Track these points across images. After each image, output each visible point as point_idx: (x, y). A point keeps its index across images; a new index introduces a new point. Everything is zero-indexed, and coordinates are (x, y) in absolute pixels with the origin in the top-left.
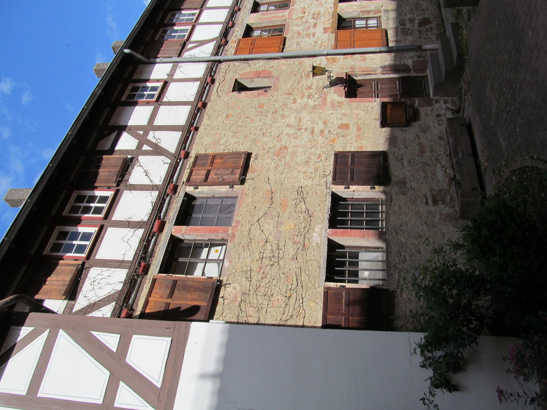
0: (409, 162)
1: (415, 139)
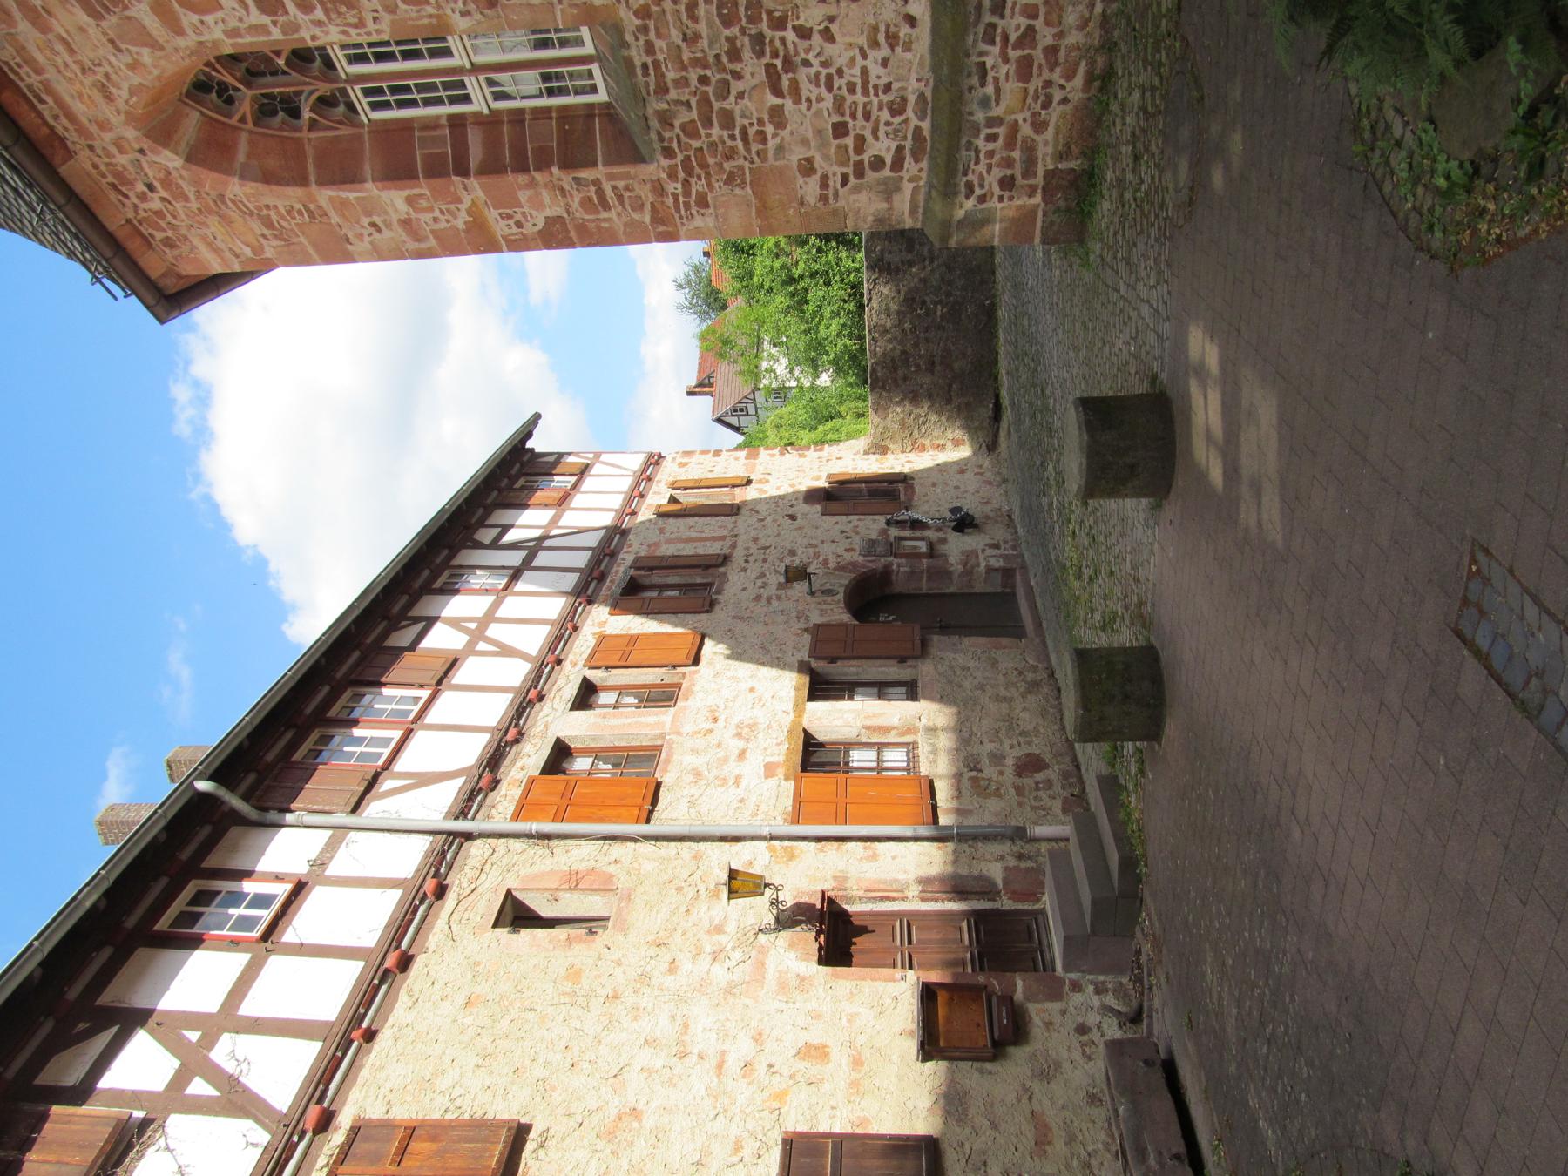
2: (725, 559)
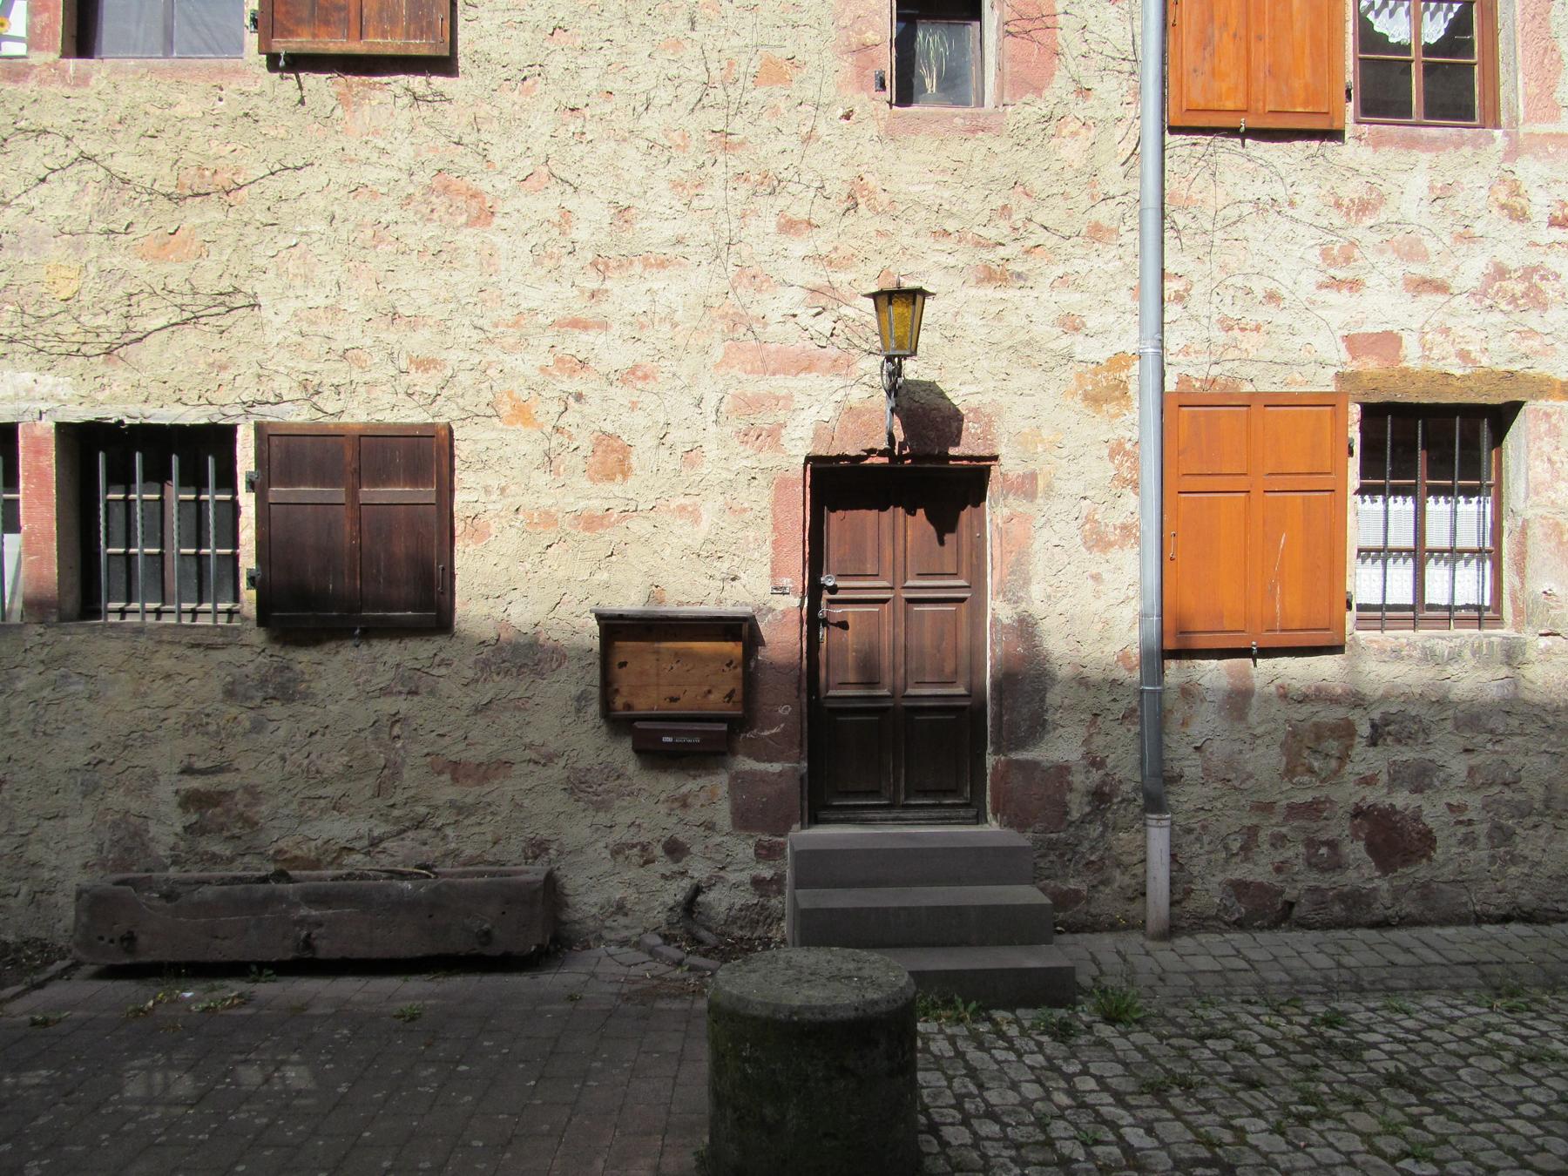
0: (396, 719)
1: (530, 746)
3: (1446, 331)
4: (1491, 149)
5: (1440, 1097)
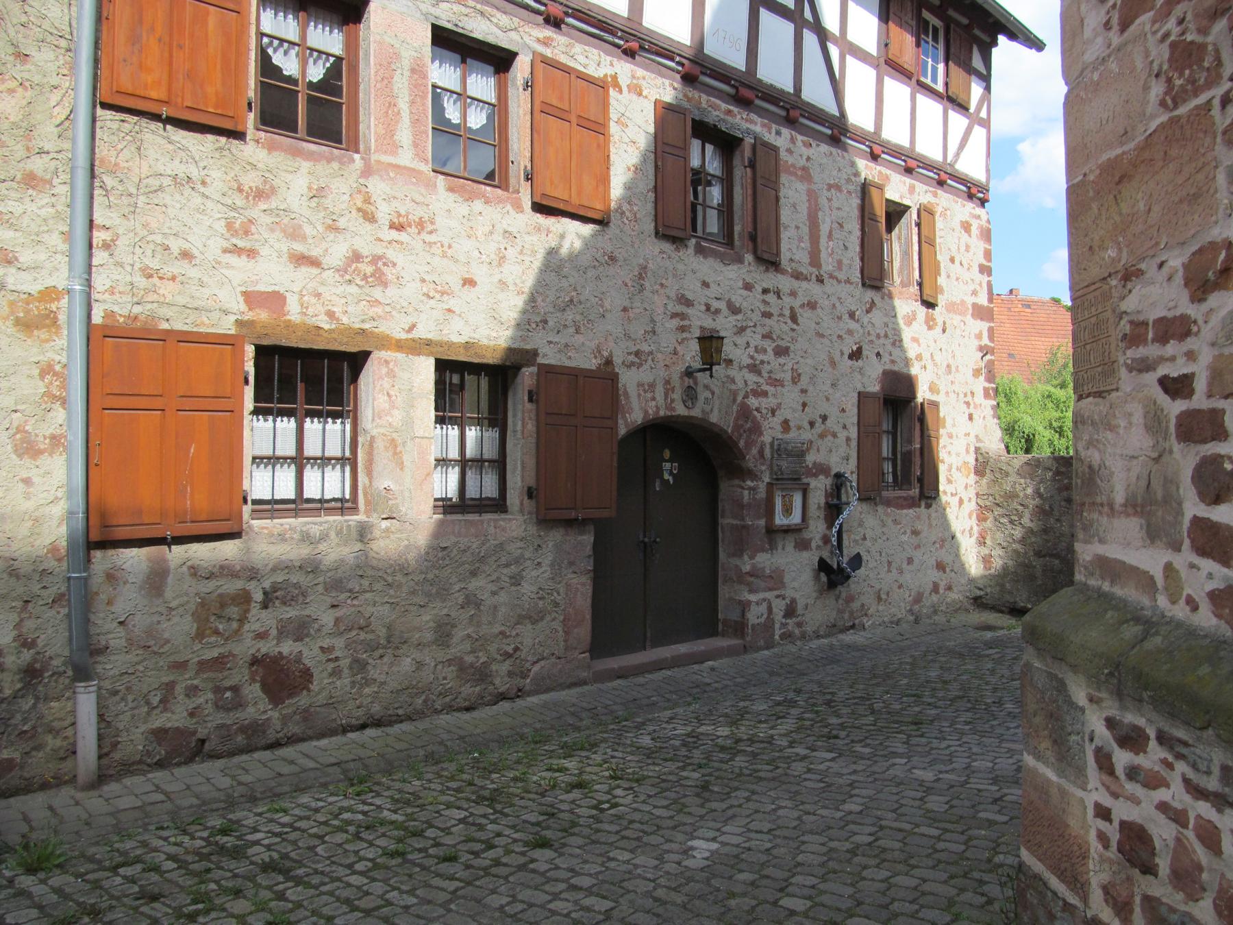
2: (771, 263)
3: (318, 295)
4: (352, 167)
5: (300, 872)
